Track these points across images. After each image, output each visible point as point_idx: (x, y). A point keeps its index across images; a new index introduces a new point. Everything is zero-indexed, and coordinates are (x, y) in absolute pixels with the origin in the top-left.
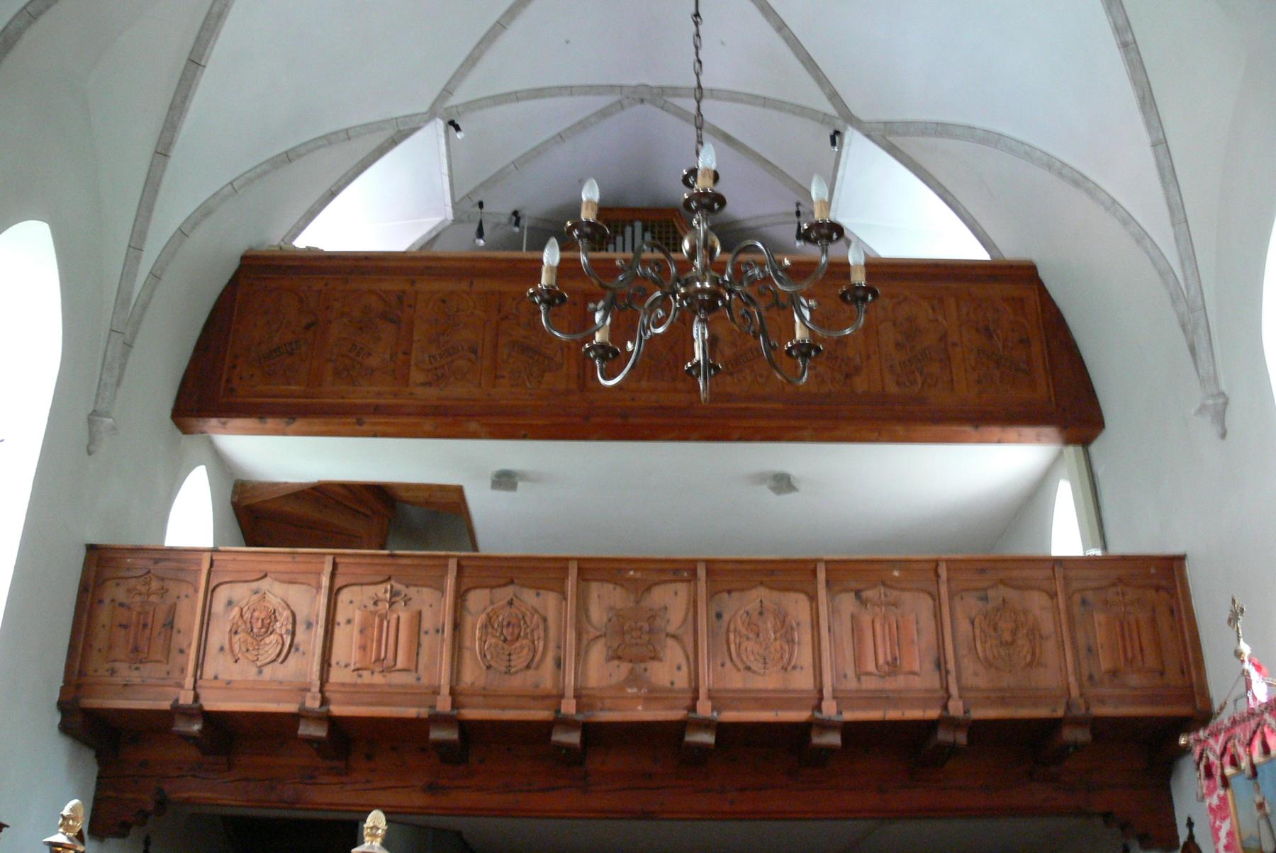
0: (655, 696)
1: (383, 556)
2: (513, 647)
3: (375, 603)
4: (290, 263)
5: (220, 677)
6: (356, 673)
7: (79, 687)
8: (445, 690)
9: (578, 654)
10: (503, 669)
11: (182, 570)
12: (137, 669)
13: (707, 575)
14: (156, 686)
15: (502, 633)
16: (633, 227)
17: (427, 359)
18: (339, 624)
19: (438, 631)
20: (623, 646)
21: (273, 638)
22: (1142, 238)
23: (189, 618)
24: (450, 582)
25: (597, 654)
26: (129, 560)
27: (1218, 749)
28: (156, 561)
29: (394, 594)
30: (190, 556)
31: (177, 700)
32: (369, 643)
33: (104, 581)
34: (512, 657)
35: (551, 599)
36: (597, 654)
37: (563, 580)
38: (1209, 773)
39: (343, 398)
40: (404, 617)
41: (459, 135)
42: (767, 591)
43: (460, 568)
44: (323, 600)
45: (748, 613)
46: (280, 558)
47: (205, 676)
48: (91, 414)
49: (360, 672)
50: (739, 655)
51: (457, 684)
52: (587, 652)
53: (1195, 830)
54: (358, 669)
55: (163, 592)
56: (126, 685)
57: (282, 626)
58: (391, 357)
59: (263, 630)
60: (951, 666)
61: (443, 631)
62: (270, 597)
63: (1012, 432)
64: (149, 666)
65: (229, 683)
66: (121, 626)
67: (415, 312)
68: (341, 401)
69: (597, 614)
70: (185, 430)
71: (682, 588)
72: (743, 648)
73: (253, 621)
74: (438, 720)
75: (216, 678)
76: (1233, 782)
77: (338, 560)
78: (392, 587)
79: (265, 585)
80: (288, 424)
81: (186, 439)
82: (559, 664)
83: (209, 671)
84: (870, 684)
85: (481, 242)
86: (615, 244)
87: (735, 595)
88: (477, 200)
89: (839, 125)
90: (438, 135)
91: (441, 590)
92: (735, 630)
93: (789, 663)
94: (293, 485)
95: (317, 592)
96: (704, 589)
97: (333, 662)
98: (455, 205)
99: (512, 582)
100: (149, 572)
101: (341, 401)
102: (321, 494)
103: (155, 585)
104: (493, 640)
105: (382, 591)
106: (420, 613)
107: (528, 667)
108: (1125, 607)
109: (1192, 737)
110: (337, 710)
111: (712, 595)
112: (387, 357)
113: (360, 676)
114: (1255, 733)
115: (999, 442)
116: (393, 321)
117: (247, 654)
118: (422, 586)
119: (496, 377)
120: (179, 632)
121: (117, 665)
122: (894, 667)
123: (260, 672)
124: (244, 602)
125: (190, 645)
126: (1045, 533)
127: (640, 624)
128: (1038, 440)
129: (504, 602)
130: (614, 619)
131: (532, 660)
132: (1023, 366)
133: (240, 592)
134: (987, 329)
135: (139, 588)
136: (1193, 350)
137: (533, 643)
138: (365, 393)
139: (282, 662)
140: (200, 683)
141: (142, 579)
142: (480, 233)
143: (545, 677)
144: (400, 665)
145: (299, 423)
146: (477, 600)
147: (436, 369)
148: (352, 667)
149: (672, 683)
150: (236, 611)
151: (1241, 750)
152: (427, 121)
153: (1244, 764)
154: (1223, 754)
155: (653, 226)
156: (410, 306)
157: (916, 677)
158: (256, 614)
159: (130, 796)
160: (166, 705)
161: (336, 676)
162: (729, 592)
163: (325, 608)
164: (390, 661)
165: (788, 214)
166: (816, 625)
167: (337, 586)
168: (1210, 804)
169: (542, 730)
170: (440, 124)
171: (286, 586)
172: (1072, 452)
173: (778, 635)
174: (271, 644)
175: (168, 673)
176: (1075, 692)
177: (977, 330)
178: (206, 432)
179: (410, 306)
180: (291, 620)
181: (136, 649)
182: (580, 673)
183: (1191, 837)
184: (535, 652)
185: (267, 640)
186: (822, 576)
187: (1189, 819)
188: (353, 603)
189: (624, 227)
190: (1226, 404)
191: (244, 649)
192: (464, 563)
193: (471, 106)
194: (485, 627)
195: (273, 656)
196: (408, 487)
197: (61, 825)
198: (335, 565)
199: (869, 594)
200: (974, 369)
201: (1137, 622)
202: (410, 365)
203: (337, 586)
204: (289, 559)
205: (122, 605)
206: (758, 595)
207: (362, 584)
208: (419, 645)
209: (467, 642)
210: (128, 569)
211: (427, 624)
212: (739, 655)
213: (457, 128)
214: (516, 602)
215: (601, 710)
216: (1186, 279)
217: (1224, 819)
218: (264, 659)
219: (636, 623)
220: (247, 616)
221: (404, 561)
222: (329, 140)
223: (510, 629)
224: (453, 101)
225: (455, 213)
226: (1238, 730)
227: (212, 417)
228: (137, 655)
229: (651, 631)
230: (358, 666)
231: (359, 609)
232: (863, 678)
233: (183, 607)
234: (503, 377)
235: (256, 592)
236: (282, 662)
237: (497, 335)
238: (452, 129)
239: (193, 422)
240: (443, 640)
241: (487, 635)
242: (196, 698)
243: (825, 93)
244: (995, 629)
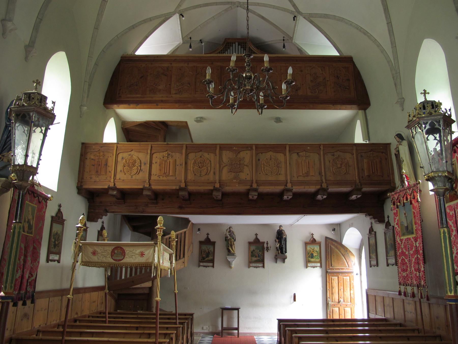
0: (241, 182)
1: (165, 144)
2: (202, 169)
3: (163, 158)
4: (136, 59)
5: (121, 179)
6: (158, 177)
7: (82, 182)
8: (183, 181)
9: (219, 171)
10: (199, 175)
11: (109, 149)
12: (98, 177)
13: (256, 148)
14: (103, 181)
15: (199, 165)
16: (235, 44)
17: (176, 87)
18: (153, 163)
19: (181, 165)
20: (232, 168)
21: (135, 167)
22: (383, 51)
23: (111, 162)
24: (184, 151)
25: (225, 171)
26: (94, 147)
27: (396, 198)
28: (101, 147)
29: (169, 155)
30: (111, 145)
31: (109, 186)
32: (162, 169)
33: (87, 153)
34: (202, 172)
35: (212, 155)
36: (225, 171)
37: (215, 150)
38: (394, 204)
39: (152, 98)
40: (171, 161)
41: (183, 19)
42: (273, 153)
43: (186, 147)
44: (149, 157)
45: (267, 159)
46: (136, 145)
47: (116, 179)
48: (81, 106)
49: (160, 177)
50: (264, 171)
51: (186, 180)
52: (222, 170)
53: (389, 218)
54: (159, 176)
55: (104, 156)
56: (95, 182)
57: (137, 164)
58: (166, 86)
59: (132, 166)
60: (323, 174)
61: (182, 165)
62: (134, 156)
63: (344, 106)
64: (101, 176)
65: (123, 180)
66: (92, 165)
67: (172, 73)
68: (151, 99)
69: (225, 159)
70: (107, 108)
71: (248, 152)
72: (265, 169)
73: (130, 163)
74: (181, 189)
75: (120, 179)
76: (399, 207)
77: (152, 146)
78: (168, 153)
79: (132, 153)
80: (137, 106)
81: (107, 110)
82: (214, 173)
83: (118, 177)
84: (301, 179)
85: (191, 49)
86: (230, 49)
87: (263, 154)
88: (189, 37)
89: (296, 14)
90: (177, 19)
91: (182, 154)
92: (263, 164)
93: (278, 173)
94: (139, 122)
95: (147, 155)
96: (255, 152)
97: (152, 174)
98: (183, 39)
99: (201, 151)
100: (99, 150)
101: (151, 99)
102: (146, 125)
103: (101, 154)
104: (196, 167)
105: (165, 154)
106: (176, 160)
107: (206, 174)
108: (373, 158)
109: (391, 194)
110: (153, 187)
111: (257, 154)
112: (165, 86)
113: (160, 178)
114: (405, 194)
115: (340, 109)
116: (166, 75)
117: (128, 172)
118: (176, 152)
119: (196, 91)
120: (109, 166)
121: (92, 176)
122: (307, 174)
123: (132, 177)
124: (127, 158)
125: (112, 170)
126: (352, 136)
127: (237, 162)
128: (351, 109)
129: (199, 156)
130: (230, 161)
131: (207, 173)
132: (347, 87)
133: (125, 155)
134: (337, 76)
135: (97, 154)
136: (395, 85)
137: (207, 167)
138: (158, 97)
139: (138, 174)
140: (115, 180)
141: (98, 152)
142: (190, 47)
143: (211, 177)
144: (170, 175)
145: (140, 106)
146: (192, 156)
147: (178, 89)
148: (157, 175)
149: (246, 179)
150: (124, 160)
151: (402, 199)
152: (174, 14)
153: (402, 203)
154: (397, 199)
155: (241, 44)
156: (170, 71)
157: (314, 177)
158: (130, 161)
159: (97, 211)
160: (106, 187)
161: (153, 178)
162: (262, 153)
163: (149, 159)
164: (168, 174)
165: (281, 40)
166: (286, 163)
167: (152, 153)
168: (394, 212)
169: (210, 193)
170: (177, 16)
171: (138, 153)
172: (361, 112)
173: (275, 165)
174: (135, 169)
175: (106, 178)
176: (358, 181)
177: (335, 77)
178: (113, 108)
179: (170, 71)
180: (140, 163)
181: (97, 172)
182: (220, 176)
183: (388, 220)
184: (208, 170)
185: (134, 168)
186: (288, 148)
187: (388, 216)
188: (157, 158)
189: (232, 44)
190: (404, 101)
191: (127, 171)
192: (187, 146)
193: (187, 9)
194: (194, 164)
195: (135, 173)
196: (171, 122)
197: (80, 222)
198: (151, 147)
199: (301, 154)
200: (333, 88)
201: (376, 161)
202: (171, 88)
203: (152, 153)
204: (139, 145)
205: (92, 159)
206: (270, 154)
207: (159, 152)
208: (176, 169)
209: (189, 168)
210: (94, 149)
211: (178, 163)
212: (264, 171)
213: (183, 16)
214: (202, 156)
215: (226, 186)
216: (395, 64)
217: (397, 217)
218: (133, 173)
219: (236, 162)
220: (128, 161)
221: (171, 146)
222: (145, 21)
223: (201, 164)
224: (182, 8)
225: (183, 41)
226: (401, 193)
227: (114, 104)
228: (98, 173)
229: (240, 164)
230: (159, 175)
231: (159, 159)
232: (299, 177)
233: (110, 160)
234: (198, 91)
235: (130, 155)
236: (138, 174)
237: (196, 79)
238: (181, 16)
239: (109, 106)
240: (182, 167)
241: (194, 165)
242: (115, 184)
243: (292, 5)
244: (336, 164)
